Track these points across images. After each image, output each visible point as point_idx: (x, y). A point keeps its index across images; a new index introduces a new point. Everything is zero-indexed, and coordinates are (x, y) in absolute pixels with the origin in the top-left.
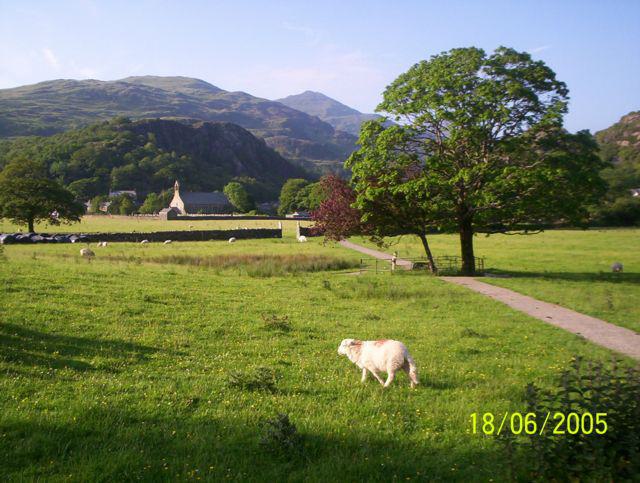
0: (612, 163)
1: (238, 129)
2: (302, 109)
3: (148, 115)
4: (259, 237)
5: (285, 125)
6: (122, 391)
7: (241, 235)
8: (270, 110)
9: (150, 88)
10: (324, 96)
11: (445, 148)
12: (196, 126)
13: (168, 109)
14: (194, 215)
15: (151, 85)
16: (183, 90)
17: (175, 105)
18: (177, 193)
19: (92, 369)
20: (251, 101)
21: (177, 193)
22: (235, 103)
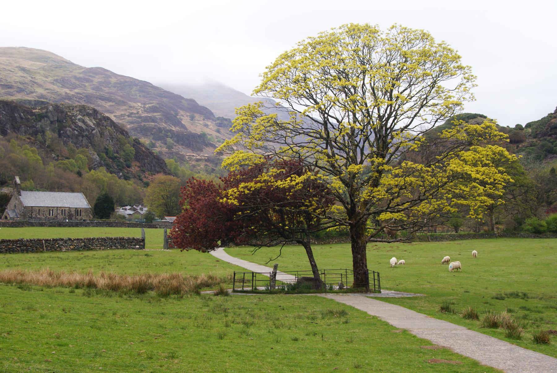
16: (27, 64)
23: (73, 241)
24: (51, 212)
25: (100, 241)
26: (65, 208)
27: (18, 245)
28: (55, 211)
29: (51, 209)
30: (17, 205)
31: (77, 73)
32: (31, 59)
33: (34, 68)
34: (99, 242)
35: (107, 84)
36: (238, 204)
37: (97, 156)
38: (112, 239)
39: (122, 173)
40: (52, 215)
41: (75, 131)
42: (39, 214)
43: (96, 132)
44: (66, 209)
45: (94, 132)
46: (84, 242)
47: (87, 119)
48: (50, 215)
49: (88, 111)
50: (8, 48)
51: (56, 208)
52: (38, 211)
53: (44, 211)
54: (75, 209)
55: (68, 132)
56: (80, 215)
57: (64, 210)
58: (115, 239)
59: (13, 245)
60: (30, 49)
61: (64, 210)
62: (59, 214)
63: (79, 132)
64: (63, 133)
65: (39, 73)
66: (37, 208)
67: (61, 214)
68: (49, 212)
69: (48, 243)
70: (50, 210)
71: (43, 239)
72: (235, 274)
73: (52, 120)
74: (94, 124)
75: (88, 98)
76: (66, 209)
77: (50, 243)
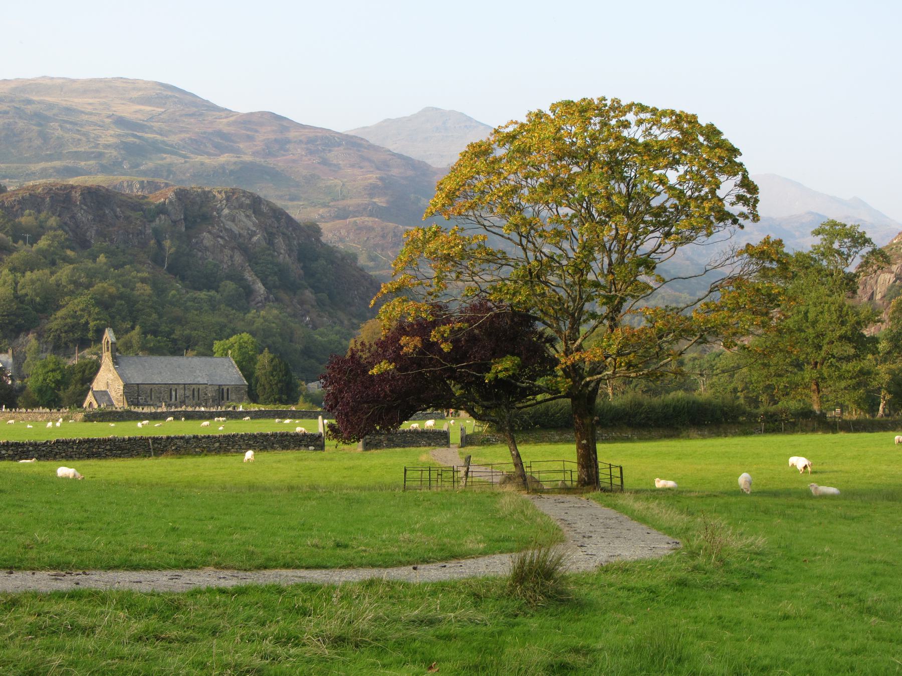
0: (296, 269)
1: (256, 204)
2: (415, 152)
3: (44, 173)
4: (285, 447)
5: (372, 190)
6: (666, 665)
7: (262, 443)
8: (335, 156)
9: (51, 106)
10: (470, 119)
11: (532, 228)
12: (158, 199)
13: (87, 156)
14: (147, 410)
15: (49, 99)
16: (128, 111)
17: (107, 146)
18: (107, 360)
19: (880, 562)
20: (292, 135)
21: (107, 360)
22: (250, 138)
23: (200, 440)
24: (174, 393)
25: (246, 438)
26: (198, 386)
27: (108, 447)
28: (180, 392)
29: (174, 389)
30: (110, 382)
31: (222, 125)
32: (132, 101)
33: (140, 116)
34: (244, 440)
35: (282, 144)
36: (370, 373)
37: (262, 287)
38: (267, 435)
39: (310, 317)
40: (176, 400)
41: (219, 239)
42: (151, 399)
43: (259, 239)
44: (200, 387)
45: (255, 239)
46: (219, 441)
47: (241, 215)
48: (171, 400)
49: (243, 199)
50: (91, 80)
51: (181, 386)
52: (149, 391)
53: (161, 393)
54: (217, 388)
55: (205, 242)
56: (228, 399)
57: (196, 390)
58: (272, 435)
59: (99, 448)
60: (134, 82)
61: (196, 390)
62: (188, 397)
63: (226, 240)
64: (197, 243)
65: (151, 128)
66: (147, 386)
67: (191, 397)
68: (169, 394)
69: (158, 444)
70: (171, 390)
71: (150, 438)
72: (405, 470)
73: (174, 218)
74: (254, 224)
75: (247, 171)
76: (200, 387)
77: (161, 444)
